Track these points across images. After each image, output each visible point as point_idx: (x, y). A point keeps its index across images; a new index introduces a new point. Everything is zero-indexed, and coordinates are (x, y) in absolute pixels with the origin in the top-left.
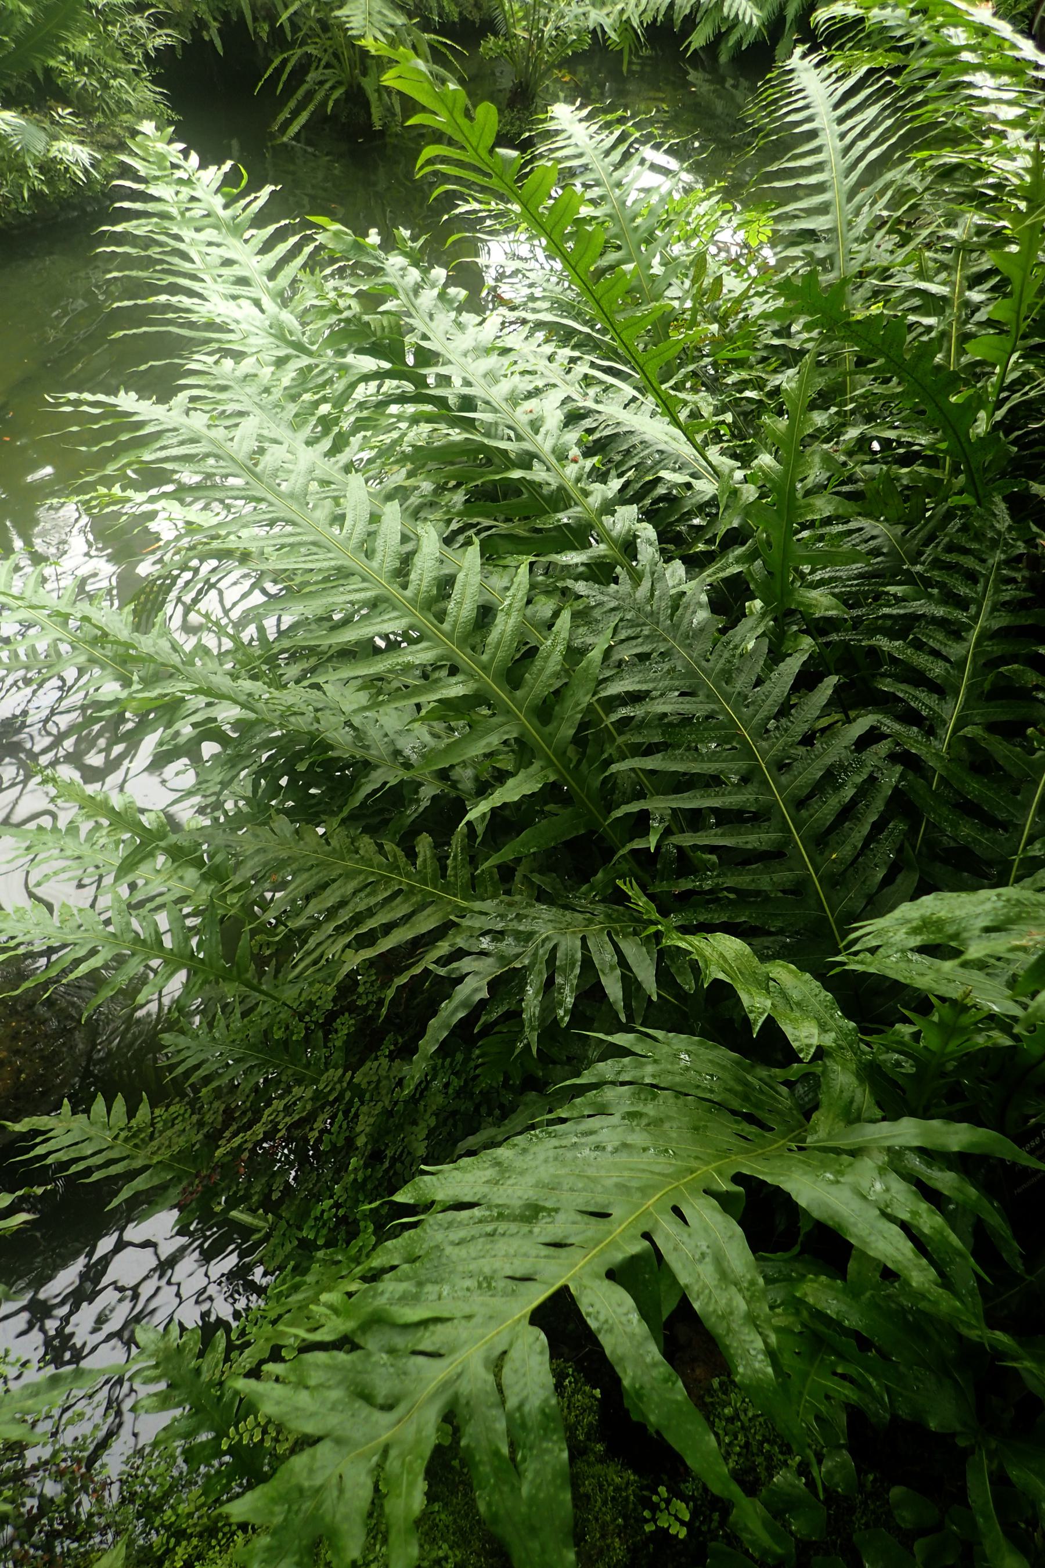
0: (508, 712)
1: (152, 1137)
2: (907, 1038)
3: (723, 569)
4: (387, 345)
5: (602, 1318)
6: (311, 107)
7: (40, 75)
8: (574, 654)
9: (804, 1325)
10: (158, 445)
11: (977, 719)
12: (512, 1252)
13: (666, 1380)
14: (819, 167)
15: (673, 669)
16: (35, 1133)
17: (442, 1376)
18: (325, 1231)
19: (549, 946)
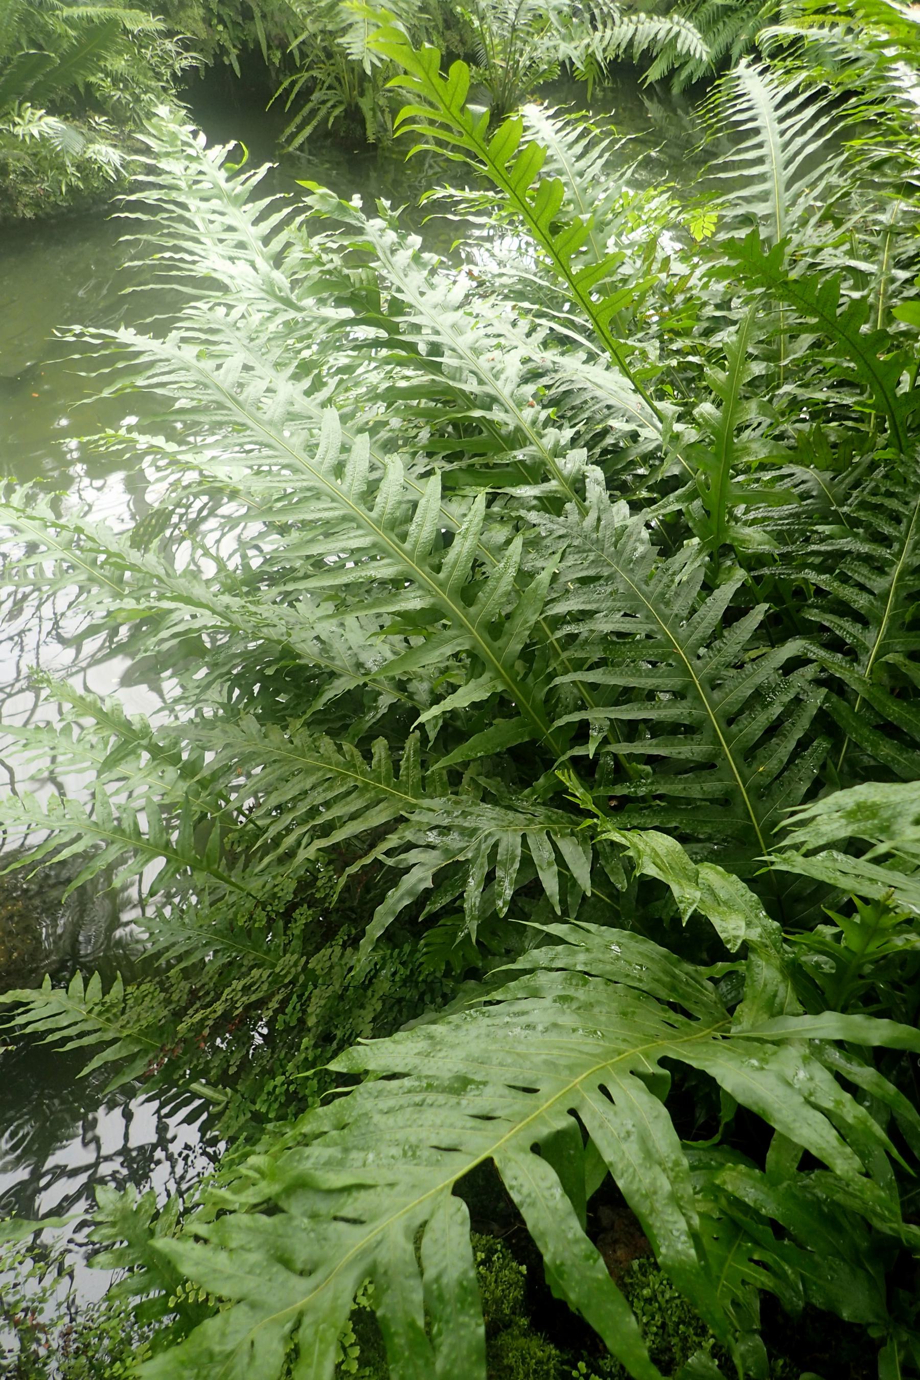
0: (462, 626)
1: (123, 1012)
2: (828, 939)
3: (664, 507)
4: (365, 301)
5: (525, 1191)
6: (314, 123)
7: (82, 90)
8: (524, 576)
9: (722, 1211)
10: (150, 373)
11: (898, 648)
12: (438, 1122)
13: (588, 1258)
14: (760, 161)
15: (616, 592)
16: (18, 1004)
17: (361, 1243)
18: (276, 1106)
19: (491, 841)
